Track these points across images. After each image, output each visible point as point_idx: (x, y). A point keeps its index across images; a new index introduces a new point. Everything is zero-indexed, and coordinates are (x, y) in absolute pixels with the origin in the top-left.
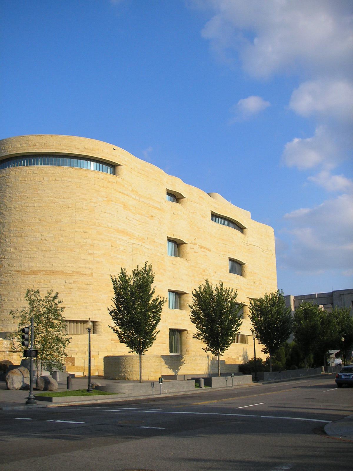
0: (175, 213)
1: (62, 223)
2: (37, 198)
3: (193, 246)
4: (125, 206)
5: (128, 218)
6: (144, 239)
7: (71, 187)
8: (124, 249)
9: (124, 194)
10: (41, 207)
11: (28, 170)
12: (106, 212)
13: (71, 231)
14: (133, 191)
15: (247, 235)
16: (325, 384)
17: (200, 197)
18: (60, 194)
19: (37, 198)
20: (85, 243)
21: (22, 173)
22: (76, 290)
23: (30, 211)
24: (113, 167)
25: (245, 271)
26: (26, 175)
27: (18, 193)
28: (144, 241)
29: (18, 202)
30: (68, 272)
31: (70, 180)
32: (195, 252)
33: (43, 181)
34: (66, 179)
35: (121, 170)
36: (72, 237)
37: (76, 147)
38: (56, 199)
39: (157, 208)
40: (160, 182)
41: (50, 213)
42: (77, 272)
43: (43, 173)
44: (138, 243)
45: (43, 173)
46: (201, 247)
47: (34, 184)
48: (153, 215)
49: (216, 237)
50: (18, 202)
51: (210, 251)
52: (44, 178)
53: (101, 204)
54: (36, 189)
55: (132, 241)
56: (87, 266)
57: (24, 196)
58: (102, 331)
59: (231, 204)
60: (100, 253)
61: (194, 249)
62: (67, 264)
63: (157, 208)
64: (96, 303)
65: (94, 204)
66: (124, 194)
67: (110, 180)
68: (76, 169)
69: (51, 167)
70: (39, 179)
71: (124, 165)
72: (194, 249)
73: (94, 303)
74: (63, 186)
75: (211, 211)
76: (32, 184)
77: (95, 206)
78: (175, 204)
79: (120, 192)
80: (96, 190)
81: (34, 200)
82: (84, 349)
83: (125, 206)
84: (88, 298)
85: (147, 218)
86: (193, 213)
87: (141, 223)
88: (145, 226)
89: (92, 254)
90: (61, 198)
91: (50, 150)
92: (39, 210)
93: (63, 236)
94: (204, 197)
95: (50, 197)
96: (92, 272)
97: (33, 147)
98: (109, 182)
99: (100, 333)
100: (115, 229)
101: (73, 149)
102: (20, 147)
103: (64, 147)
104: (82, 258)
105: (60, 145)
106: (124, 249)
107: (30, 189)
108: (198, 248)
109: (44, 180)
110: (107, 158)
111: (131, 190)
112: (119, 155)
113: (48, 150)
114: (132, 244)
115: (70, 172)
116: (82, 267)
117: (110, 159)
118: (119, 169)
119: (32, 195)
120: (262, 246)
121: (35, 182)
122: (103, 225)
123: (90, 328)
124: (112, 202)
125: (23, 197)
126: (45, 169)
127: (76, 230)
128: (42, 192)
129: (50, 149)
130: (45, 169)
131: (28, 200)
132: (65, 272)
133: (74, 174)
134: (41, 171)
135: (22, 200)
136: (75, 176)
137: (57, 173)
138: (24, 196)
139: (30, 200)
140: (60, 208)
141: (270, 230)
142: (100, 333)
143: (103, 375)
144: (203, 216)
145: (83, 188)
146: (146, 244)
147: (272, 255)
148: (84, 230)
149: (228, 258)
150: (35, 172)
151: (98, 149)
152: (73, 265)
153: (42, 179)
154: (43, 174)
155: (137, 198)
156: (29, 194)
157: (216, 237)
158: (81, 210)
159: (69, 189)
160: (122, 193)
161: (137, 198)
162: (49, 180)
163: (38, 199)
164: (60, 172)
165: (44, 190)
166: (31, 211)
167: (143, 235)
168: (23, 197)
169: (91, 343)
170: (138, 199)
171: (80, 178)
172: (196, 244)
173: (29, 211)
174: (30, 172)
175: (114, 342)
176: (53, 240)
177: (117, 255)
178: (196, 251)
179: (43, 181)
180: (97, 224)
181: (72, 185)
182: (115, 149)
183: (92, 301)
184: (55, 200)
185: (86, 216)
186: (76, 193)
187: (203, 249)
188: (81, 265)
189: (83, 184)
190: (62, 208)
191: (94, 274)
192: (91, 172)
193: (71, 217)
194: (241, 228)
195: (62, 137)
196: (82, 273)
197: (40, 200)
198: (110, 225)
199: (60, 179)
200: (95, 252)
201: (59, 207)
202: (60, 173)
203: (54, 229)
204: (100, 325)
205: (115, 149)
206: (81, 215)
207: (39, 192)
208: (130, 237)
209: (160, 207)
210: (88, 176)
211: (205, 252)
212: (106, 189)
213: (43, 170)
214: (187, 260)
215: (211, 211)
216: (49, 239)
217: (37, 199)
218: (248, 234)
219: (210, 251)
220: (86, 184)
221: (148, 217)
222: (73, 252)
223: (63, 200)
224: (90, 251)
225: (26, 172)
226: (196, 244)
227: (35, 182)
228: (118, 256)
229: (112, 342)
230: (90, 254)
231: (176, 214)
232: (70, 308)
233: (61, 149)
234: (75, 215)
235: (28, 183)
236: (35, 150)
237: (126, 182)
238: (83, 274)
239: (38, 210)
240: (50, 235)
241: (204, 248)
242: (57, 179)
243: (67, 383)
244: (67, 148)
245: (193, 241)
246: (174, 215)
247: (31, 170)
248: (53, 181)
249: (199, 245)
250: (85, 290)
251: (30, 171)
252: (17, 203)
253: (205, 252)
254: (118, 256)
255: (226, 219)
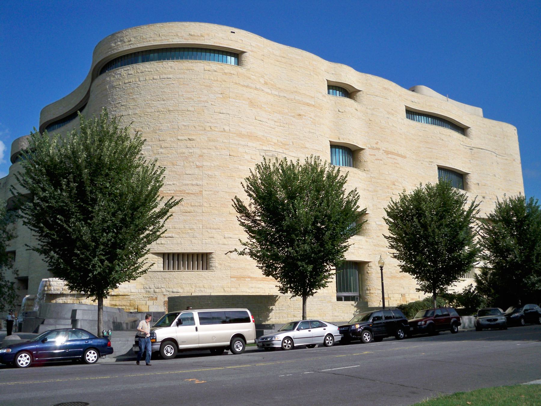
0: (340, 110)
1: (161, 131)
2: (131, 105)
3: (373, 151)
4: (252, 104)
5: (258, 118)
6: (288, 145)
7: (172, 85)
8: (251, 159)
9: (251, 88)
10: (137, 114)
11: (123, 72)
12: (222, 112)
13: (172, 139)
14: (266, 83)
15: (471, 136)
16: (419, 343)
17: (385, 88)
18: (158, 95)
19: (131, 105)
20: (191, 154)
21: (117, 77)
22: (180, 213)
23: (124, 121)
24: (237, 55)
25: (469, 183)
26: (121, 78)
27: (112, 101)
28: (287, 147)
29: (112, 112)
30: (169, 192)
31: (171, 76)
32: (376, 159)
33: (139, 83)
34: (166, 76)
35: (247, 58)
36: (174, 148)
37: (179, 34)
38: (153, 102)
39: (308, 105)
40: (313, 71)
41: (147, 121)
42: (180, 191)
43: (138, 73)
44: (276, 150)
45: (139, 72)
46: (387, 153)
47: (128, 88)
48: (302, 113)
49: (415, 140)
50: (112, 112)
51: (405, 157)
52: (140, 78)
53: (213, 103)
54: (131, 93)
55: (265, 148)
56: (194, 182)
57: (118, 103)
58: (217, 265)
59: (448, 99)
60: (212, 165)
61: (375, 155)
62: (167, 182)
63: (308, 105)
64: (207, 230)
65: (203, 103)
66: (251, 88)
67: (226, 71)
68: (179, 62)
69: (148, 64)
70: (134, 81)
71: (250, 52)
72: (375, 155)
73: (203, 230)
74: (163, 86)
75: (406, 106)
76: (126, 88)
77: (205, 105)
78: (347, 100)
79: (244, 86)
80: (207, 86)
81: (129, 108)
82: (190, 289)
83: (252, 104)
84: (196, 223)
85: (292, 118)
86: (373, 109)
87: (281, 124)
88: (289, 128)
89: (201, 167)
90: (159, 100)
91: (147, 43)
92: (135, 118)
93: (163, 147)
94: (391, 89)
95: (147, 100)
96: (202, 190)
97: (128, 43)
98: (225, 74)
99: (214, 268)
100: (235, 133)
101: (174, 38)
102: (115, 47)
103: (163, 38)
104: (187, 172)
105: (158, 36)
106: (251, 159)
107: (124, 95)
108: (383, 154)
109: (139, 81)
110: (221, 44)
111: (263, 82)
112: (240, 40)
113: (145, 43)
114: (264, 151)
115: (171, 67)
116: (188, 185)
117: (226, 45)
118: (246, 58)
119: (127, 101)
120: (496, 149)
121: (129, 86)
122: (216, 129)
123: (382, 266)
124: (230, 99)
125: (117, 105)
126: (141, 68)
127: (179, 138)
128: (137, 96)
129: (147, 41)
130: (141, 68)
131: (123, 108)
132: (165, 192)
133: (176, 69)
134: (137, 71)
135: (117, 109)
136: (177, 71)
137: (155, 70)
138: (118, 103)
139: (125, 108)
140: (158, 113)
141: (511, 131)
142: (214, 268)
143: (369, 306)
144: (389, 113)
145: (188, 85)
146: (291, 151)
147: (514, 160)
148: (190, 137)
149: (437, 166)
150: (130, 72)
151: (208, 35)
152: (175, 182)
153: (137, 80)
154: (138, 74)
155: (275, 92)
156: (123, 101)
157: (415, 140)
158: (186, 112)
159: (170, 88)
160: (247, 87)
161: (275, 92)
162: (146, 80)
163: (133, 105)
164: (159, 68)
165: (140, 94)
166: (125, 120)
167: (285, 140)
168: (117, 105)
169: (384, 281)
170: (277, 93)
171: (184, 73)
172: (378, 149)
173: (123, 121)
174: (124, 74)
175: (235, 279)
176: (151, 153)
177: (239, 166)
178: (380, 158)
179: (139, 83)
180: (209, 129)
181: (173, 83)
182: (234, 33)
183: (201, 228)
184: (152, 104)
185: (192, 119)
186: (178, 92)
187: (390, 156)
188: (185, 182)
189: (188, 79)
190: (161, 112)
191: (204, 192)
192: (199, 64)
193: (173, 122)
194: (462, 129)
195: (161, 25)
196: (187, 191)
197: (135, 105)
198: (227, 128)
199: (159, 77)
200: (205, 164)
201: (157, 112)
202: (158, 70)
203: (152, 139)
204: (213, 258)
205: (234, 33)
206: (185, 119)
207: (134, 96)
208: (261, 143)
209: (313, 103)
210: (195, 69)
211: (394, 159)
212: (221, 83)
213: (139, 68)
214: (364, 170)
215: (406, 106)
216: (145, 152)
217: (132, 106)
218: (472, 135)
219: (405, 157)
220: (192, 80)
221: (293, 117)
222: (175, 166)
223: (163, 102)
224: (198, 164)
225: (120, 74)
226: (378, 149)
227: (130, 85)
228: (240, 167)
229: (232, 279)
230: (198, 167)
231: (343, 111)
232: (171, 237)
233: (160, 41)
234: (177, 119)
235: (122, 88)
236: (131, 47)
237: (253, 72)
238: (188, 193)
239: (133, 119)
240: (146, 148)
241: (392, 153)
242: (155, 77)
243: (56, 329)
244: (168, 38)
245: (375, 146)
246: (339, 113)
247: (126, 72)
248: (151, 81)
249: (383, 151)
250: (192, 214)
251: (125, 73)
252: (111, 114)
253: (394, 159)
254: (240, 167)
255: (336, 87)
